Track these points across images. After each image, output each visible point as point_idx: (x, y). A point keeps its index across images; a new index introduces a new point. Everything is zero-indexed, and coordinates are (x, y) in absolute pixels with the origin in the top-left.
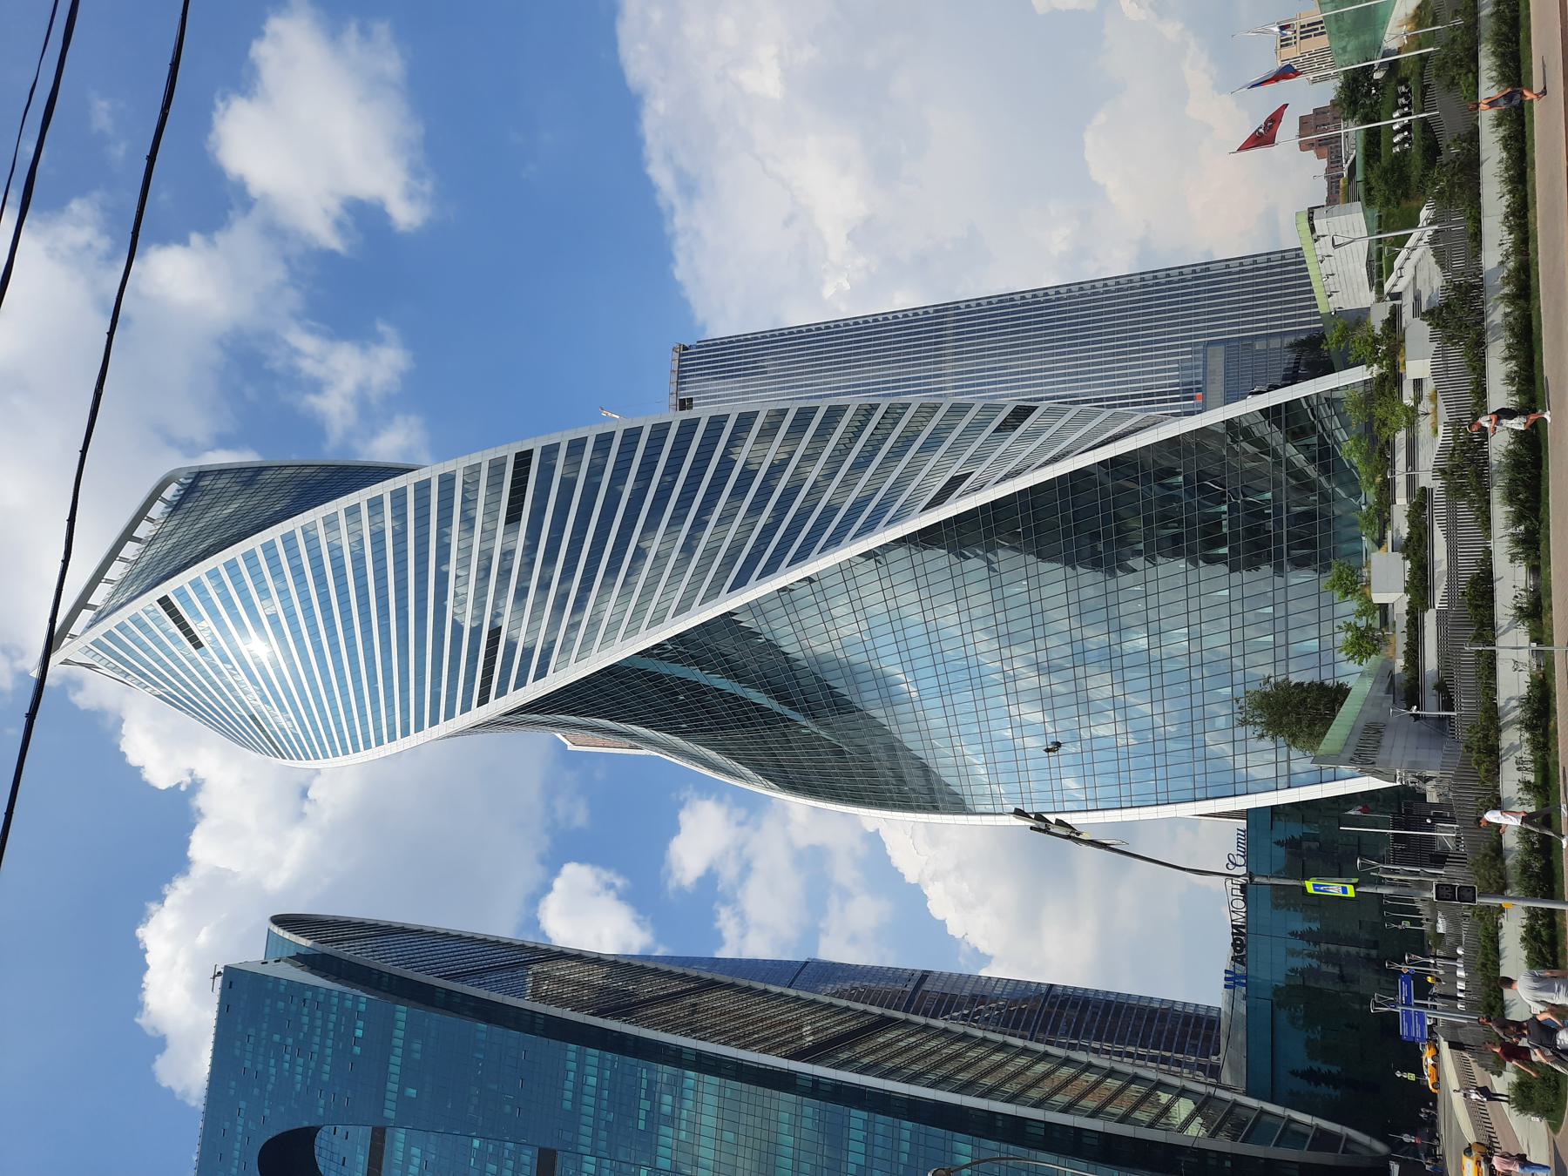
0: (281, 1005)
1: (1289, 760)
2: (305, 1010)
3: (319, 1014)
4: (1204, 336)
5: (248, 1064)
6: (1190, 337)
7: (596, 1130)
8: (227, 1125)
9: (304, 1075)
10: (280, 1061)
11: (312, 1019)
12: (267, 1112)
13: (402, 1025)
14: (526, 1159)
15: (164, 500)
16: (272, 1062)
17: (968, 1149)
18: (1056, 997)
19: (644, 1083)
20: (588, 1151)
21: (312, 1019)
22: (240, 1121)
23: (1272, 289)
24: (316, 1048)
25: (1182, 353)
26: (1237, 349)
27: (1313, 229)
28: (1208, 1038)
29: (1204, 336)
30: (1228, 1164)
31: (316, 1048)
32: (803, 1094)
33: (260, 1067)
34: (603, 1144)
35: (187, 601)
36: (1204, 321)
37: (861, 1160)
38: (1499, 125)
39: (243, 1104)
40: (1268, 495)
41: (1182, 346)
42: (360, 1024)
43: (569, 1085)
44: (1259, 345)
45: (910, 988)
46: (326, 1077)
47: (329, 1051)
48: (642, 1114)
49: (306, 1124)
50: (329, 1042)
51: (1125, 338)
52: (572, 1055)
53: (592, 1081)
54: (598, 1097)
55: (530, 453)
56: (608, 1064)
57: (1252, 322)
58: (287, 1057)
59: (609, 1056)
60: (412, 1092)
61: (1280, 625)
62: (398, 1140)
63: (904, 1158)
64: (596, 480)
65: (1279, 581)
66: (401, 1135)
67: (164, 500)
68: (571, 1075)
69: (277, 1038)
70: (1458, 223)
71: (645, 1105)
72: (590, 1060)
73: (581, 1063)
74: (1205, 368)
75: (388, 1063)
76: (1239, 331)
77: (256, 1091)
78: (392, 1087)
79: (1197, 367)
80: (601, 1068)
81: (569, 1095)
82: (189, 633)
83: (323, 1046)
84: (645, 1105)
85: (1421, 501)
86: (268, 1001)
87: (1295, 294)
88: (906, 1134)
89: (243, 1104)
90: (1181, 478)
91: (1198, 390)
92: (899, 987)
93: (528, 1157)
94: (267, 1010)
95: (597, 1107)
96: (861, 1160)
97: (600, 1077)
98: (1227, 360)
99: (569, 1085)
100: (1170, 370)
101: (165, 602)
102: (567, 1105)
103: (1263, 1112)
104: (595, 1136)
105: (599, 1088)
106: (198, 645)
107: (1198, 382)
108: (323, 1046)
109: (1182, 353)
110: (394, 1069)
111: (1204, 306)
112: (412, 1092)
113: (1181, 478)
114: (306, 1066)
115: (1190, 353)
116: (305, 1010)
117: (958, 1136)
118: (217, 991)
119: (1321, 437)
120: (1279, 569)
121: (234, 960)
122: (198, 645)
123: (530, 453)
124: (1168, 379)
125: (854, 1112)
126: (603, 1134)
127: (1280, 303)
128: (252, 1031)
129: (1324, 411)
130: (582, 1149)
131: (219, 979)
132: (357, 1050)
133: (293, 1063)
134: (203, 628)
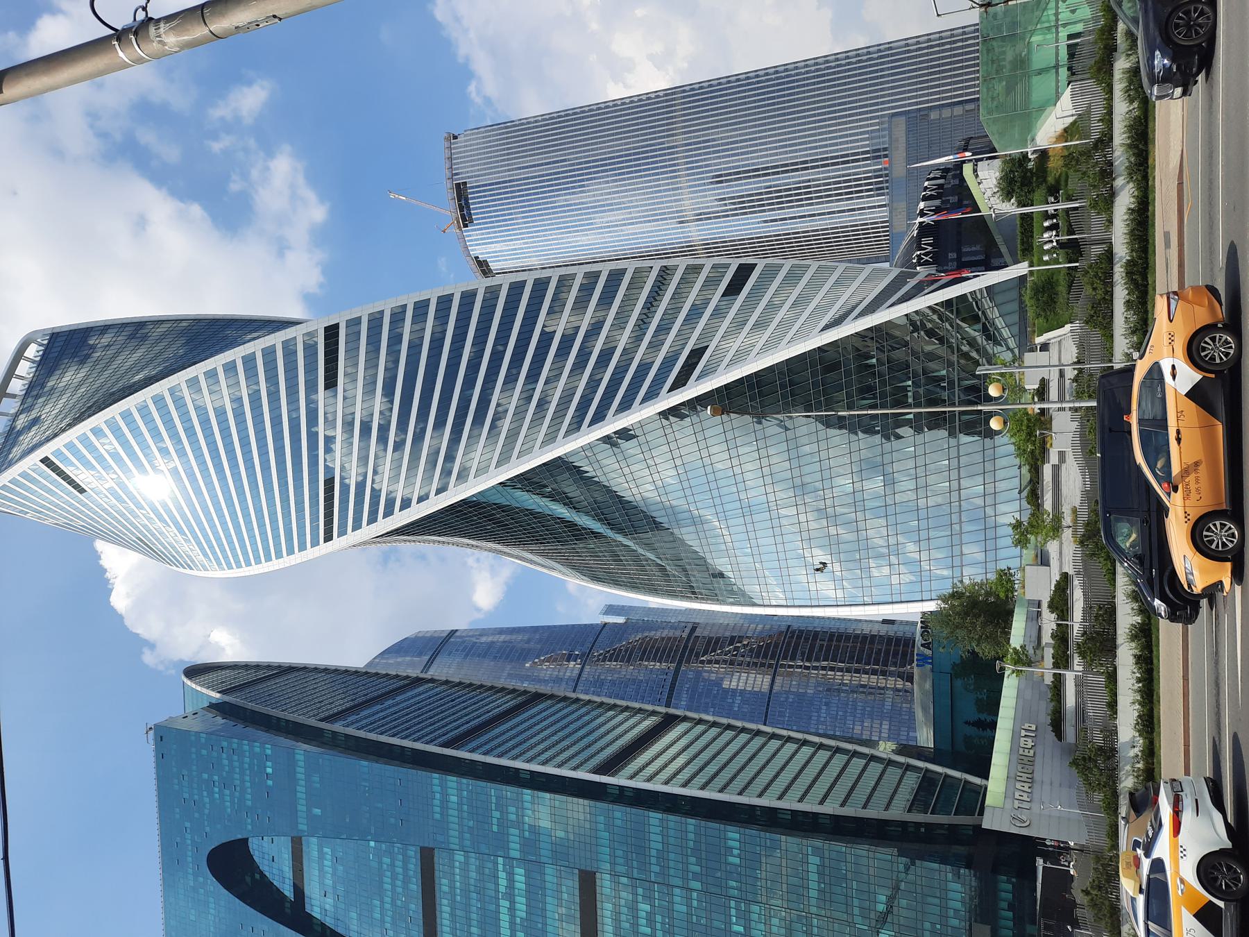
0: (204, 752)
1: (961, 522)
2: (224, 756)
3: (235, 758)
4: (889, 108)
5: (186, 796)
6: (877, 111)
7: (461, 833)
8: (178, 839)
9: (232, 802)
10: (211, 793)
11: (231, 761)
12: (208, 829)
13: (302, 764)
14: (412, 853)
15: (28, 359)
16: (205, 794)
17: (737, 836)
18: (793, 632)
19: (494, 799)
20: (457, 847)
21: (231, 761)
22: (188, 836)
23: (944, 85)
24: (237, 782)
25: (871, 125)
26: (917, 119)
27: (977, 176)
28: (904, 654)
29: (889, 108)
30: (923, 830)
31: (237, 782)
32: (613, 802)
33: (196, 797)
34: (468, 843)
35: (65, 459)
36: (889, 75)
37: (660, 846)
38: (1133, 333)
39: (188, 824)
40: (944, 372)
41: (871, 118)
42: (269, 764)
43: (437, 802)
44: (934, 115)
45: (685, 635)
46: (249, 803)
47: (248, 784)
48: (495, 821)
49: (240, 837)
50: (247, 778)
51: (824, 114)
52: (436, 781)
53: (454, 799)
54: (460, 810)
55: (336, 326)
56: (464, 787)
57: (928, 95)
58: (216, 790)
59: (464, 781)
60: (317, 811)
61: (954, 475)
62: (312, 847)
63: (691, 844)
64: (397, 348)
65: (953, 442)
66: (314, 840)
67: (28, 359)
68: (438, 796)
69: (205, 776)
70: (1096, 336)
71: (497, 814)
72: (450, 784)
73: (444, 787)
74: (890, 137)
75: (296, 791)
76: (917, 104)
77: (197, 815)
78: (302, 808)
79: (883, 136)
80: (460, 790)
81: (437, 809)
82: (71, 482)
83: (243, 781)
84: (497, 814)
85: (1062, 455)
86: (194, 750)
87: (962, 68)
88: (691, 828)
89: (188, 824)
90: (874, 361)
91: (886, 156)
92: (678, 633)
93: (414, 853)
94: (194, 756)
95: (460, 818)
96: (660, 846)
97: (460, 797)
98: (908, 131)
99: (437, 802)
100: (862, 140)
101: (46, 461)
102: (437, 816)
103: (947, 776)
104: (461, 838)
105: (460, 804)
106: (82, 491)
107: (885, 149)
108: (243, 781)
109: (871, 125)
110: (301, 795)
111: (888, 82)
112: (317, 811)
113: (874, 361)
114: (232, 796)
115: (878, 124)
116: (224, 756)
117: (729, 828)
118: (152, 742)
119: (984, 324)
120: (952, 434)
121: (160, 718)
122: (82, 491)
123: (336, 326)
124: (864, 145)
125: (651, 814)
126: (467, 836)
127: (950, 77)
128: (185, 772)
129: (987, 303)
130: (452, 846)
131: (151, 733)
132: (270, 783)
133: (220, 792)
134: (81, 476)
